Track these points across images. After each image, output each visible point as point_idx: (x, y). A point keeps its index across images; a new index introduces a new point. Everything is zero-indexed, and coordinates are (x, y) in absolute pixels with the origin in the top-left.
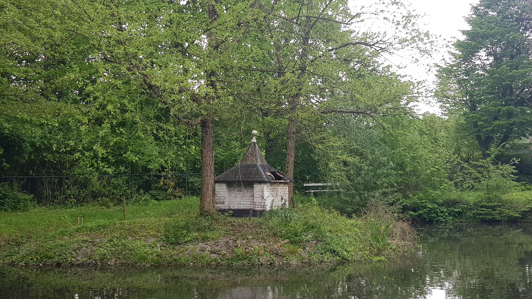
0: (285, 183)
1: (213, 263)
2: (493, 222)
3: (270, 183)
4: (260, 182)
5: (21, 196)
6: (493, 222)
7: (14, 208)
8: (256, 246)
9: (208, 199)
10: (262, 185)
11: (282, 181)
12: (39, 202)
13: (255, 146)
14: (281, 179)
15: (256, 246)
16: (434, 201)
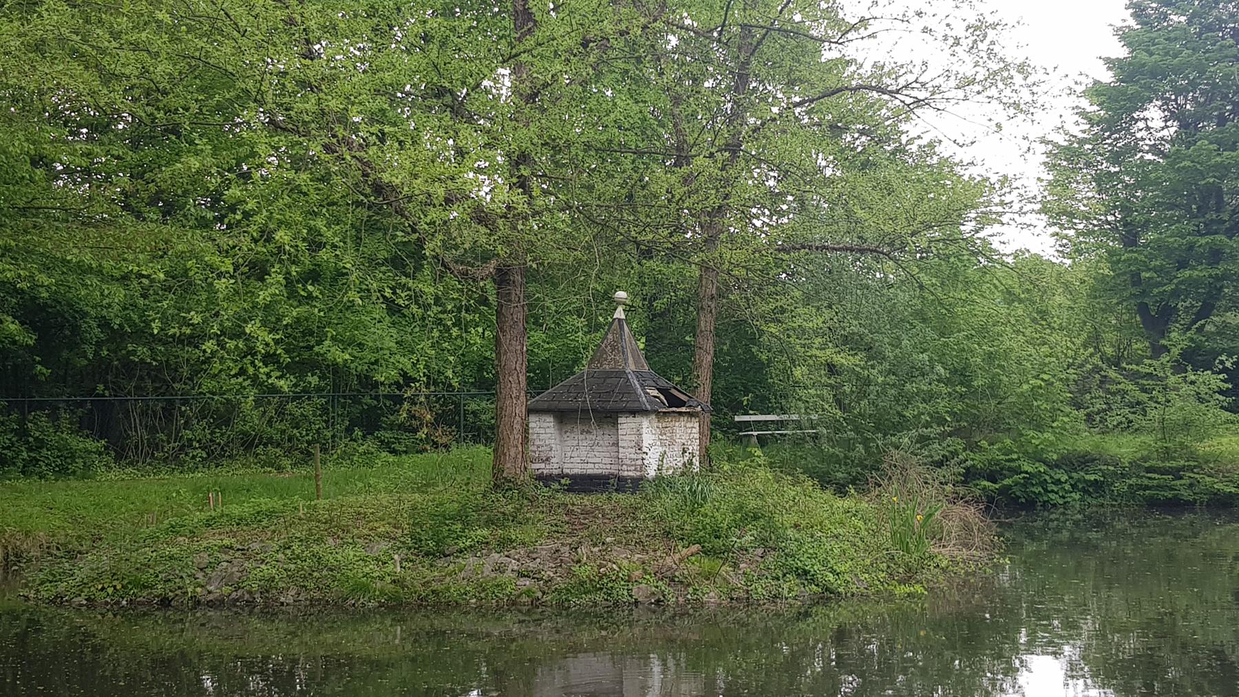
0: (691, 415)
1: (524, 599)
2: (1175, 505)
3: (657, 413)
4: (634, 413)
5: (78, 443)
6: (1175, 505)
7: (62, 472)
8: (625, 560)
9: (513, 451)
10: (638, 419)
11: (683, 409)
12: (118, 458)
13: (621, 328)
14: (683, 404)
15: (625, 560)
16: (1037, 457)
